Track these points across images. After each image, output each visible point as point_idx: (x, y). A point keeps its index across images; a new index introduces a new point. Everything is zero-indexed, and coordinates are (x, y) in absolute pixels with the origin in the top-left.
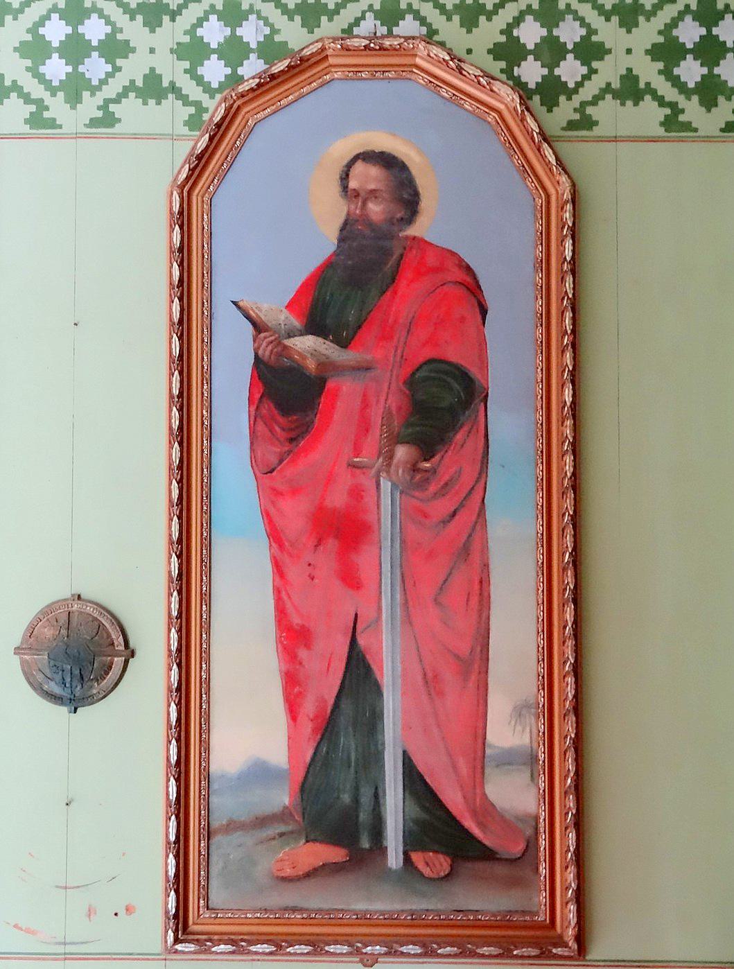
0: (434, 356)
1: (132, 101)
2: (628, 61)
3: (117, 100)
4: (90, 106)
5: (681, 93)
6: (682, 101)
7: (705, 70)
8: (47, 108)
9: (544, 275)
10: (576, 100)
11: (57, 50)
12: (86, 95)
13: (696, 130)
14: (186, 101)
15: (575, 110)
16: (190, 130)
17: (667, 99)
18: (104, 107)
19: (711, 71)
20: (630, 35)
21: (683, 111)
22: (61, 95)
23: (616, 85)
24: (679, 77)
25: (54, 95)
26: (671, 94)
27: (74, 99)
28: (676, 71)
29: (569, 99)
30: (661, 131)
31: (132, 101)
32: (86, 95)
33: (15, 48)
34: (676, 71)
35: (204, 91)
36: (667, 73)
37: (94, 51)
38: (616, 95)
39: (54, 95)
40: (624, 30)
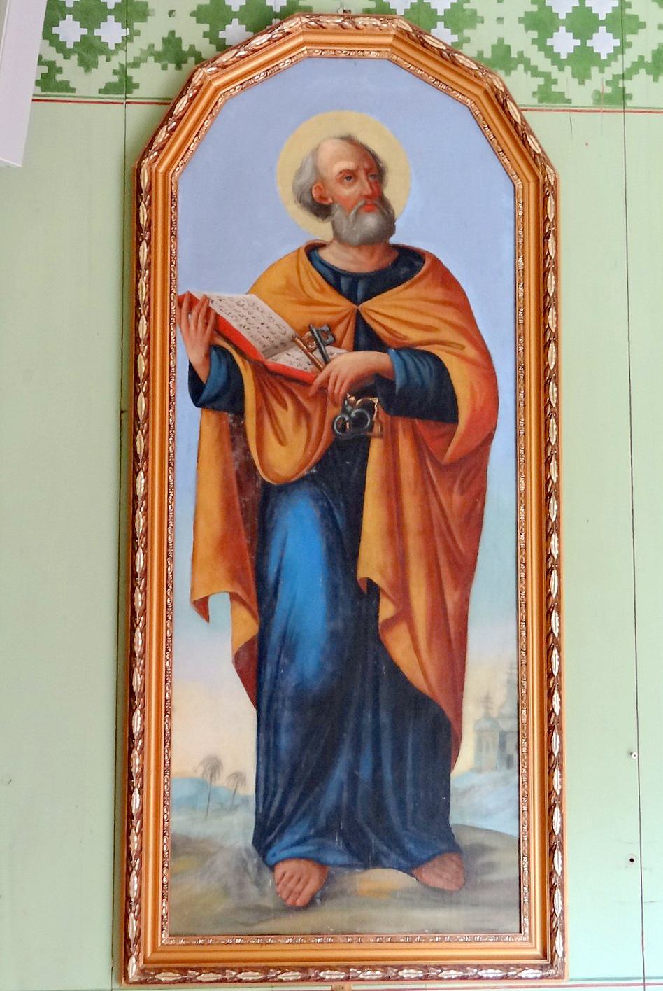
0: (276, 616)
1: (642, 77)
2: (171, 24)
3: (136, 64)
4: (598, 80)
5: (58, 51)
6: (554, 71)
7: (85, 31)
8: (555, 82)
9: (168, 363)
10: (609, 73)
11: (91, 30)
12: (594, 70)
13: (569, 101)
14: (535, 72)
15: (115, 72)
16: (42, 91)
17: (540, 69)
18: (122, 71)
19: (584, 43)
20: (647, 24)
21: (555, 82)
22: (568, 69)
23: (159, 47)
24: (58, 36)
25: (561, 69)
26: (544, 64)
27: (87, 64)
28: (549, 42)
29: (602, 71)
30: (535, 101)
31: (642, 77)
32: (594, 70)
33: (204, 33)
34: (549, 42)
35: (553, 64)
36: (541, 44)
37: (586, 44)
38: (158, 57)
39: (561, 69)
40: (522, 15)
